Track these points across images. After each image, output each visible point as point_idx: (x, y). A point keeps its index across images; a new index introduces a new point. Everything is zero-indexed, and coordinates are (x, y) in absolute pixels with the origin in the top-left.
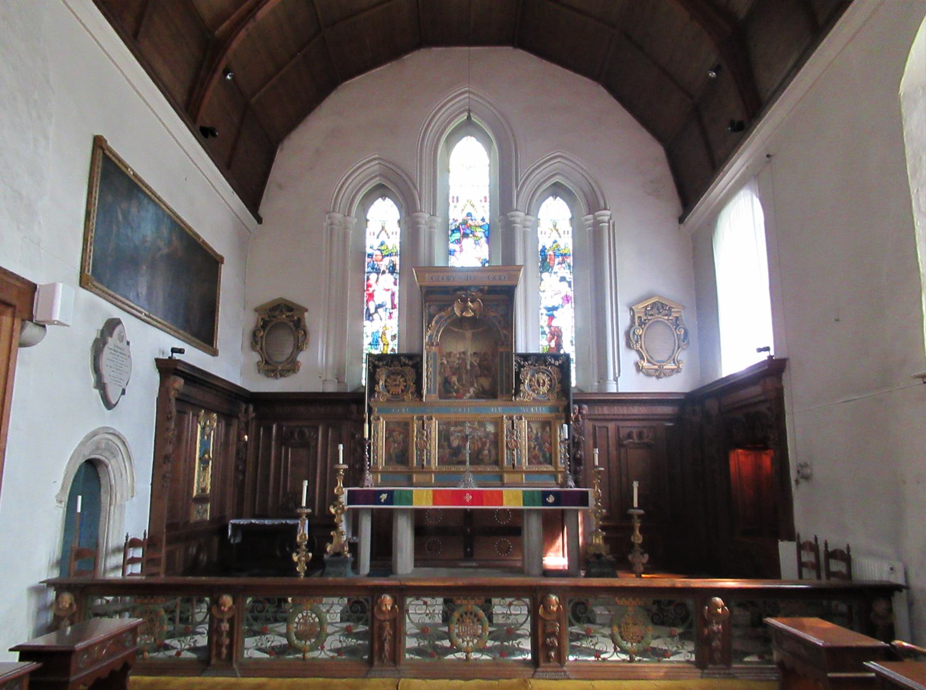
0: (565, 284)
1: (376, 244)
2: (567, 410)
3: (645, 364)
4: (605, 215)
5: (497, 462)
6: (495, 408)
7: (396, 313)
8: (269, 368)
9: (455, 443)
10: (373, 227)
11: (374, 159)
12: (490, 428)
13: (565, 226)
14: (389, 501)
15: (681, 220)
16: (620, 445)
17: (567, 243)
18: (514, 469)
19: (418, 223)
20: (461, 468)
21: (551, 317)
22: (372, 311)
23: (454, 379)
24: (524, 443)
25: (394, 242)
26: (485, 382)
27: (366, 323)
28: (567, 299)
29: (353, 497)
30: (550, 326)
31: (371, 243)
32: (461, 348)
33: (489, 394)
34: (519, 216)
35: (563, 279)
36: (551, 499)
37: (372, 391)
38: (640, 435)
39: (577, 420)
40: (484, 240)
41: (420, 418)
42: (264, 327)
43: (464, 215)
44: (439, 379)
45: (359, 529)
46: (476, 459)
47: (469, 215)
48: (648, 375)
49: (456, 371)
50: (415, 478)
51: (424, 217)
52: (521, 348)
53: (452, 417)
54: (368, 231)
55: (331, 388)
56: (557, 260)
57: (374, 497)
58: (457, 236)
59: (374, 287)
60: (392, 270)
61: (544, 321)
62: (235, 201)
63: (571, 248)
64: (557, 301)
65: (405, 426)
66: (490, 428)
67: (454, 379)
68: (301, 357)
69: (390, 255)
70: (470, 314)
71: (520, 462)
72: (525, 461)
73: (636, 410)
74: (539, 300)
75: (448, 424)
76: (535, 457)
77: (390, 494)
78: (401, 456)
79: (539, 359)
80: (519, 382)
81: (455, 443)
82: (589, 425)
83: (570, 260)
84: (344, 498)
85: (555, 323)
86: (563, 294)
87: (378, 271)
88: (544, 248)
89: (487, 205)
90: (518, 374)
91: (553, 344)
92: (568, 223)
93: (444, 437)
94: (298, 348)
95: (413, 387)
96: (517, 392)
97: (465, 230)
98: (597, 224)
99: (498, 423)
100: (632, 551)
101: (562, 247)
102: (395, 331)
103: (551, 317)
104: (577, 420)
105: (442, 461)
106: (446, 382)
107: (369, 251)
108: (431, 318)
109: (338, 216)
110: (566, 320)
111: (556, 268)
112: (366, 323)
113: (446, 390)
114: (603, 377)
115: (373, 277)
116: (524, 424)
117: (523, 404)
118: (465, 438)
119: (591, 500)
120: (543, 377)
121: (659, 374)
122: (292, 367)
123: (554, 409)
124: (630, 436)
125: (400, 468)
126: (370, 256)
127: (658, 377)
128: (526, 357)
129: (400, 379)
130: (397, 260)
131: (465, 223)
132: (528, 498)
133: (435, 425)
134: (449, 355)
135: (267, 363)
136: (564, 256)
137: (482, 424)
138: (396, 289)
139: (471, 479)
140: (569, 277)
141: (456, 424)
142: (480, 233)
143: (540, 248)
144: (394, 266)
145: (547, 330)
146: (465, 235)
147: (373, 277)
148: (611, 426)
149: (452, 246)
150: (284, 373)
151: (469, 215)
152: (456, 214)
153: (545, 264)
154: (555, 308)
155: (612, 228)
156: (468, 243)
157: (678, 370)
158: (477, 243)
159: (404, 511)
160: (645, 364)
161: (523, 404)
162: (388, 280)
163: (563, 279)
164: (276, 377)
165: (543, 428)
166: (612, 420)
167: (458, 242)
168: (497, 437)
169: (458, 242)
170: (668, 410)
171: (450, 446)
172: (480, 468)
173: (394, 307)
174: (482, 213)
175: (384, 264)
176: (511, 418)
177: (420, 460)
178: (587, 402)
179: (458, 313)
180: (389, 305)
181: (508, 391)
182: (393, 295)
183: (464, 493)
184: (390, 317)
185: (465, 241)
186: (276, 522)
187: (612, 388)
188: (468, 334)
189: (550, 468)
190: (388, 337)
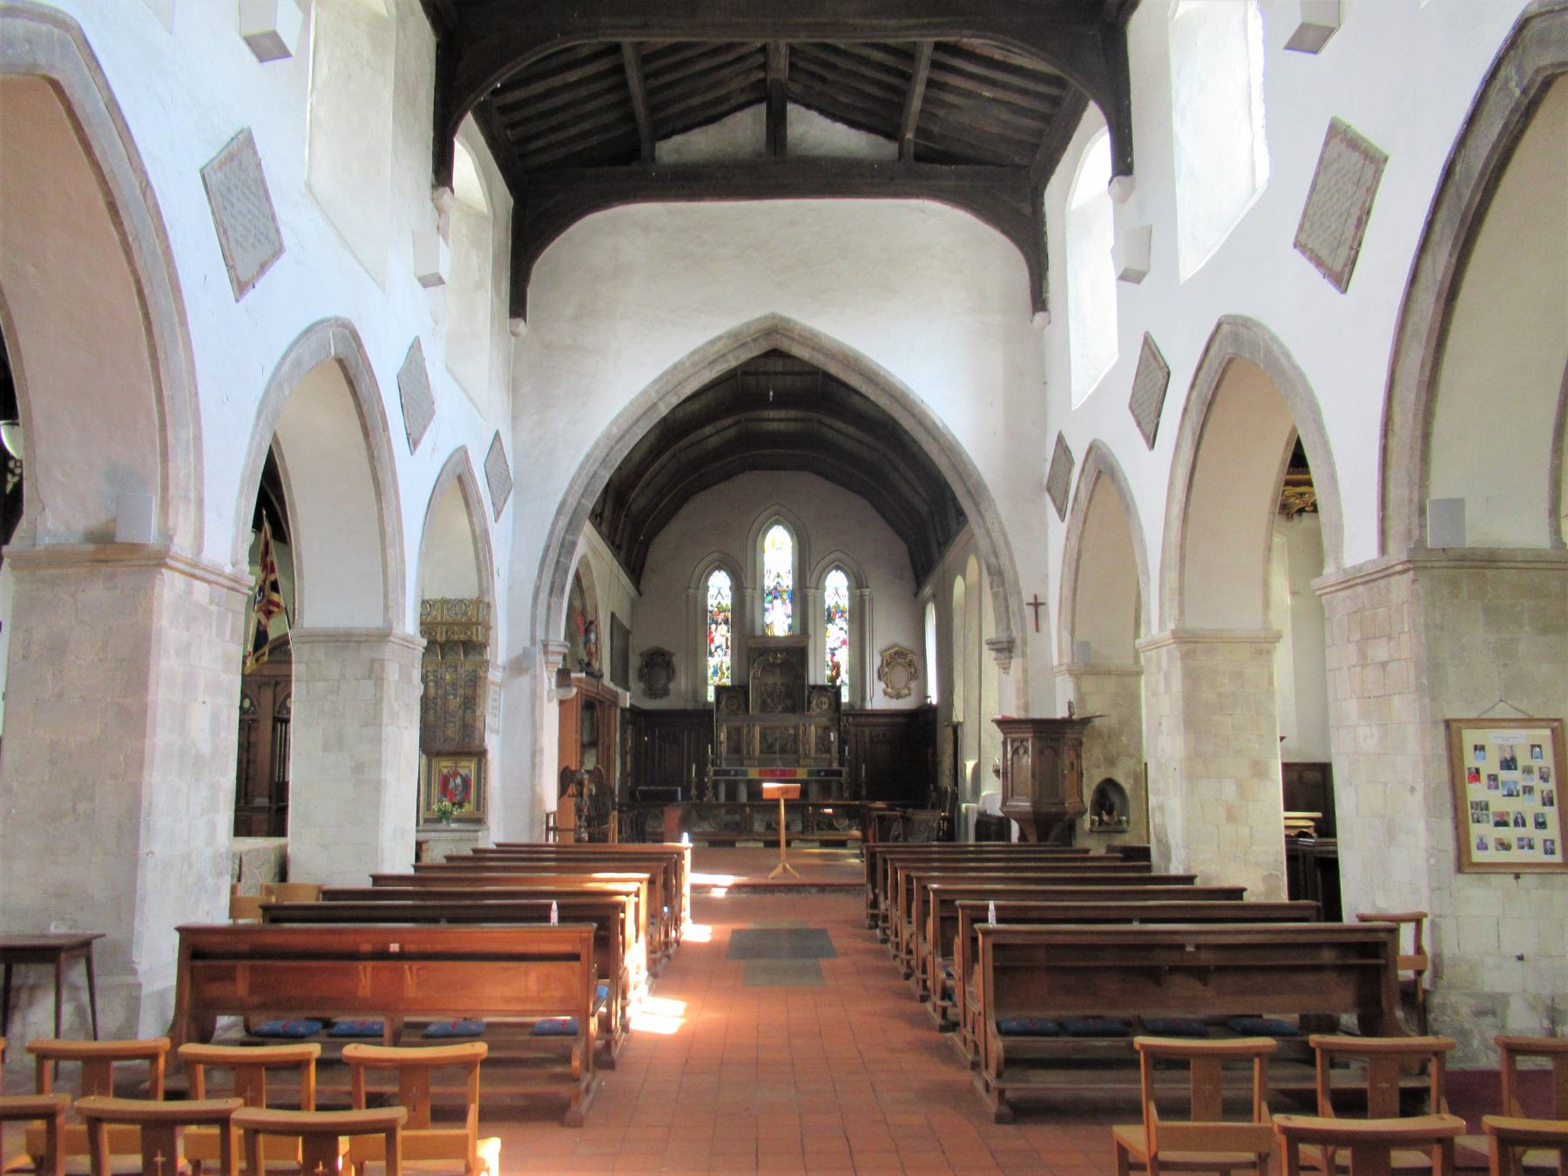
0: (843, 632)
1: (715, 603)
2: (839, 720)
3: (889, 690)
4: (867, 591)
5: (796, 752)
6: (793, 719)
7: (729, 652)
8: (652, 692)
9: (770, 741)
10: (712, 591)
11: (714, 552)
12: (792, 731)
13: (844, 592)
14: (736, 774)
15: (916, 595)
16: (872, 742)
17: (845, 603)
18: (806, 756)
19: (745, 596)
20: (774, 756)
21: (833, 655)
22: (713, 650)
23: (769, 700)
24: (813, 739)
25: (727, 601)
26: (789, 703)
27: (709, 658)
28: (844, 642)
29: (716, 773)
30: (832, 661)
31: (712, 603)
32: (774, 681)
33: (791, 709)
34: (811, 592)
35: (841, 629)
36: (823, 774)
37: (718, 708)
38: (884, 736)
39: (845, 726)
40: (788, 601)
41: (749, 725)
42: (646, 666)
43: (775, 583)
44: (759, 700)
45: (289, 1058)
46: (783, 750)
47: (778, 583)
48: (891, 697)
49: (771, 695)
50: (745, 762)
51: (749, 592)
52: (812, 681)
53: (768, 724)
54: (709, 594)
55: (690, 706)
56: (837, 616)
57: (727, 773)
58: (770, 598)
59: (714, 634)
60: (726, 622)
61: (828, 657)
62: (625, 579)
63: (847, 607)
64: (837, 644)
65: (739, 730)
66: (792, 731)
67: (769, 700)
68: (672, 686)
69: (724, 611)
70: (779, 661)
71: (809, 751)
72: (813, 751)
73: (881, 720)
74: (824, 643)
75: (766, 728)
76: (820, 749)
77: (736, 771)
78: (736, 749)
79: (822, 688)
80: (809, 702)
81: (770, 741)
82: (853, 730)
83: (847, 615)
84: (711, 774)
85: (835, 659)
86: (841, 639)
87: (716, 623)
88: (829, 608)
89: (791, 576)
90: (809, 697)
91: (834, 673)
92: (845, 589)
93: (763, 736)
94: (669, 679)
95: (743, 707)
96: (809, 709)
97: (776, 593)
98: (862, 596)
99: (796, 728)
100: (170, 533)
101: (841, 606)
102: (729, 664)
103: (833, 655)
104: (845, 726)
105: (762, 751)
106: (764, 703)
107: (710, 608)
108: (754, 661)
109: (692, 591)
110: (843, 657)
111: (837, 621)
112: (709, 658)
113: (764, 707)
114: (863, 699)
115: (713, 627)
116: (813, 728)
117: (811, 717)
118: (776, 739)
119: (844, 774)
120: (825, 699)
121: (898, 696)
122: (665, 692)
123: (832, 720)
124: (878, 736)
125: (736, 756)
126: (711, 612)
127: (897, 698)
128: (814, 687)
129: (735, 701)
130: (729, 615)
131: (775, 588)
132: (810, 773)
133: (757, 729)
134: (766, 684)
135: (650, 689)
136: (843, 612)
137: (787, 729)
138: (729, 635)
139: (779, 763)
140: (846, 627)
141: (770, 728)
142: (785, 596)
143: (826, 607)
144: (727, 620)
145: (830, 664)
146: (776, 598)
147: (713, 627)
148: (867, 730)
149: (767, 605)
150: (661, 696)
151: (778, 583)
152: (769, 583)
153: (830, 619)
154: (835, 649)
155: (871, 601)
156: (777, 603)
157: (910, 694)
158: (784, 603)
159: (742, 781)
160: (889, 690)
161: (811, 717)
162: (723, 629)
163: (841, 629)
164: (656, 698)
165: (824, 731)
166: (868, 726)
167: (771, 602)
168: (796, 736)
169: (771, 602)
170: (901, 720)
171: (767, 742)
172: (785, 756)
173: (727, 647)
174: (788, 582)
175: (721, 617)
176: (804, 725)
177: (748, 753)
178: (851, 715)
179: (771, 661)
180: (724, 646)
181: (803, 708)
182: (727, 639)
183: (776, 770)
184: (725, 655)
185: (775, 602)
186: (665, 788)
187: (869, 706)
188: (778, 671)
189: (828, 756)
190: (724, 668)
